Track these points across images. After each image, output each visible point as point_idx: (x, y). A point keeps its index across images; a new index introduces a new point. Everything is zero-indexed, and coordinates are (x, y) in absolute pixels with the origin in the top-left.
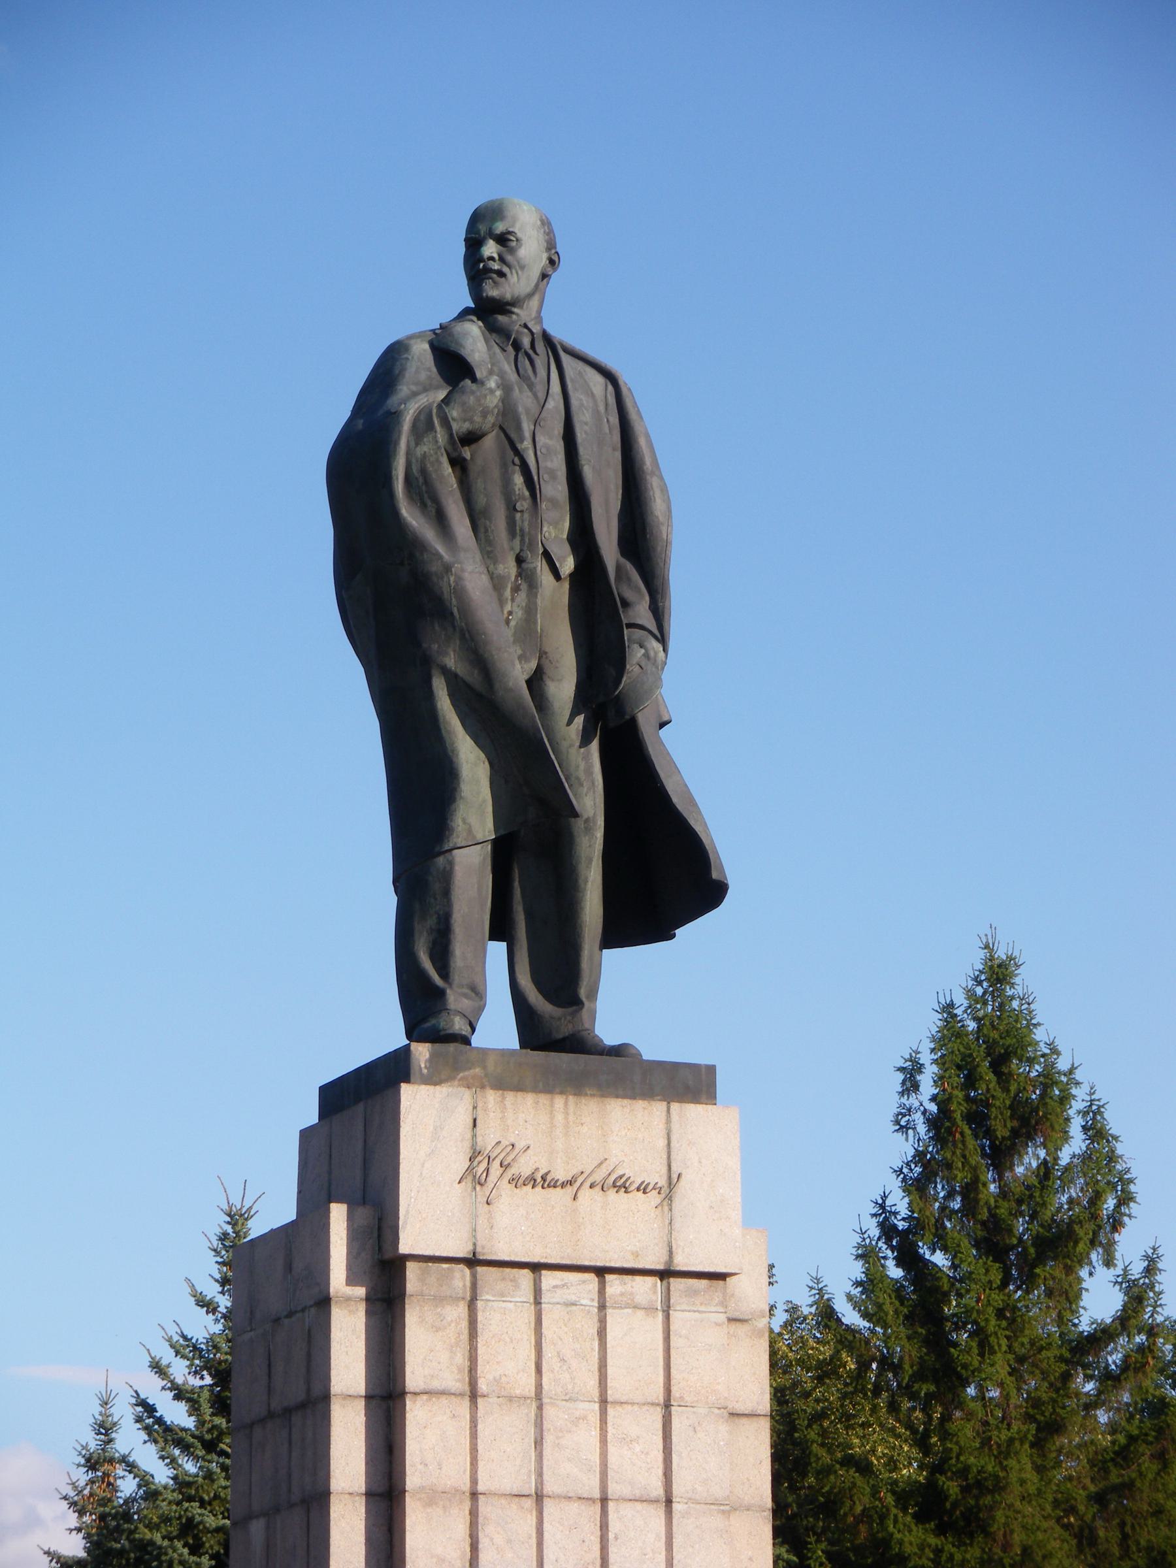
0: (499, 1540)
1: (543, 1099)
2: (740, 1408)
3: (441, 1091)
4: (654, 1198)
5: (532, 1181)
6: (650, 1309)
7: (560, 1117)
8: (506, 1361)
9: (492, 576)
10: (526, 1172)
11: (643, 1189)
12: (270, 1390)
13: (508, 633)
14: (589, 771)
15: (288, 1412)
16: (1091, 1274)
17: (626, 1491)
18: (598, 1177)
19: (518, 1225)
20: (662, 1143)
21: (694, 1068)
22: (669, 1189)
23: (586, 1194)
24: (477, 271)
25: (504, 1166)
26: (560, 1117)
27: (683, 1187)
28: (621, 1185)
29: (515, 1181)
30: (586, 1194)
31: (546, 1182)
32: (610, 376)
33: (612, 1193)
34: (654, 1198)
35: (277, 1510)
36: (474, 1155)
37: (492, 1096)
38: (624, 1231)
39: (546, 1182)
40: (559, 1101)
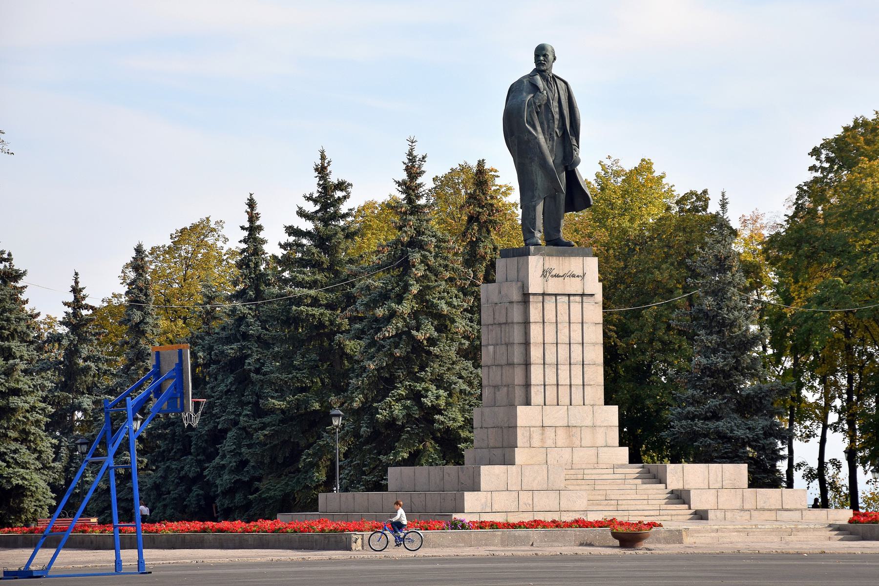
15: (500, 324)
24: (537, 61)
28: (574, 276)
29: (552, 276)
31: (558, 276)
39: (557, 276)
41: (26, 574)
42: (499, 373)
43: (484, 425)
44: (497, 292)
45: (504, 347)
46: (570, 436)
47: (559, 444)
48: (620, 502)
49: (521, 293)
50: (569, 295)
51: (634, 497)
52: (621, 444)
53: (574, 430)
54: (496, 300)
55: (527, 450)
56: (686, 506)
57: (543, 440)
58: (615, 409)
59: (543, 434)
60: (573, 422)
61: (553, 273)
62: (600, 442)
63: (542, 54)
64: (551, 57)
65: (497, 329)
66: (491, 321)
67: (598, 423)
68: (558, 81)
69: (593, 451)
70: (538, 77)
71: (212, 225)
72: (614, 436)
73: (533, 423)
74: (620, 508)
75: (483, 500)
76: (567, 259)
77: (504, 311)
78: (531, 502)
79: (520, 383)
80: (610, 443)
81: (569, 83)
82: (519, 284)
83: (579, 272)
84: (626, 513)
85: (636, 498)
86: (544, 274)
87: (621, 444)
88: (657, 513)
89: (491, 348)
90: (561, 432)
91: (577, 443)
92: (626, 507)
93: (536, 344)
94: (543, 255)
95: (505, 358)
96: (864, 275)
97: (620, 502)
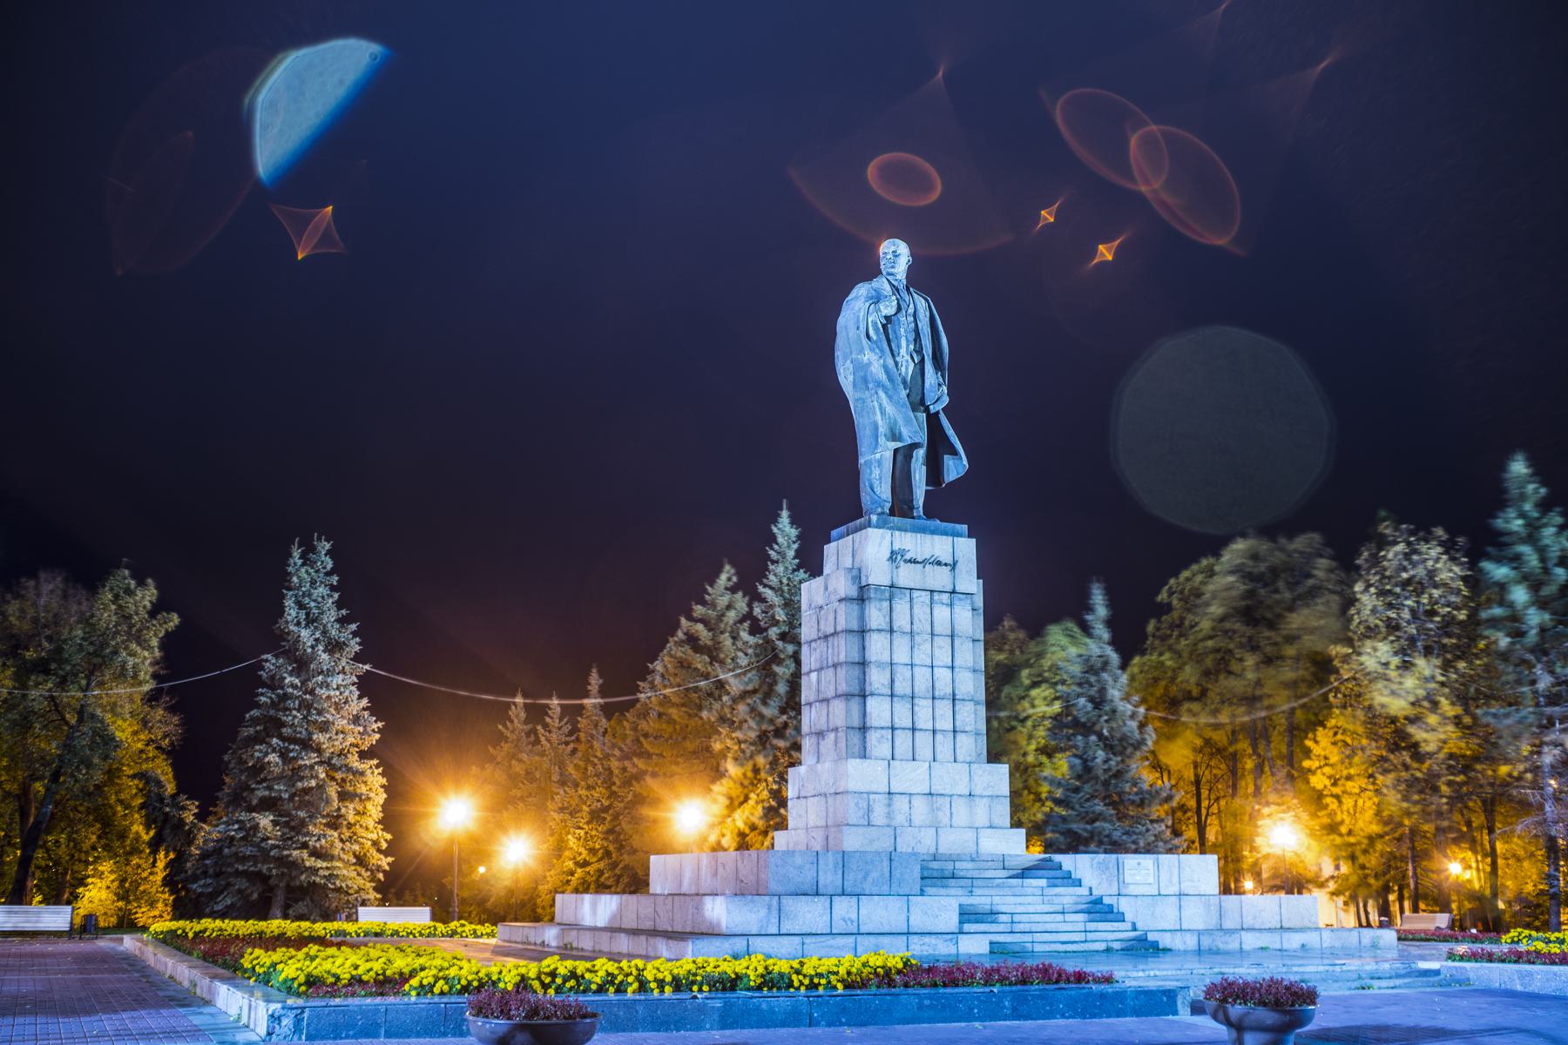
15: (826, 637)
19: (907, 576)
28: (939, 563)
31: (915, 562)
39: (915, 562)
41: (1031, 983)
42: (824, 712)
43: (803, 794)
45: (831, 670)
46: (934, 810)
47: (917, 820)
51: (1040, 908)
53: (940, 799)
54: (821, 602)
55: (861, 830)
57: (889, 816)
58: (1004, 769)
61: (908, 557)
65: (821, 645)
66: (814, 635)
71: (494, 978)
73: (874, 788)
74: (1018, 928)
77: (831, 617)
78: (854, 916)
80: (996, 821)
83: (947, 559)
84: (1027, 938)
85: (1044, 916)
86: (894, 556)
88: (1081, 937)
89: (814, 676)
90: (920, 805)
91: (946, 820)
92: (1027, 927)
93: (880, 665)
94: (891, 528)
95: (832, 687)
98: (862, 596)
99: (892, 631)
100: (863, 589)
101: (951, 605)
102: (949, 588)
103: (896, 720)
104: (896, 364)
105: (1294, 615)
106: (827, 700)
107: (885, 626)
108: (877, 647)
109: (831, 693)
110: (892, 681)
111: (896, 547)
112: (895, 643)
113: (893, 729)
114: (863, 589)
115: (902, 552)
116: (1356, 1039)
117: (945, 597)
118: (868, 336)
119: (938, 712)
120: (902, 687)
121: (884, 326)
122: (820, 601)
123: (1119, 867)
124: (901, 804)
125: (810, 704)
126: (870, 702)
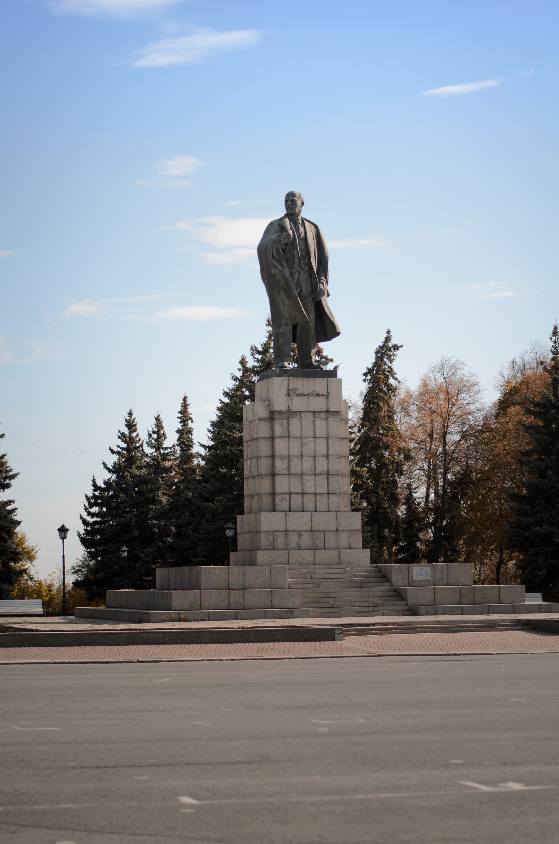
0: (143, 650)
1: (302, 378)
2: (343, 437)
3: (282, 378)
4: (325, 397)
5: (300, 395)
6: (324, 419)
7: (305, 382)
8: (295, 429)
9: (290, 272)
10: (299, 393)
11: (323, 395)
12: (250, 435)
13: (293, 283)
14: (312, 310)
15: (254, 440)
16: (192, 422)
17: (319, 454)
18: (313, 393)
19: (297, 404)
20: (326, 386)
21: (333, 326)
22: (328, 396)
23: (311, 397)
24: (288, 207)
25: (295, 392)
26: (305, 382)
27: (331, 395)
28: (318, 395)
29: (297, 395)
30: (311, 397)
31: (303, 395)
32: (316, 226)
33: (316, 397)
34: (325, 397)
35: (252, 458)
36: (288, 390)
37: (291, 378)
38: (319, 404)
39: (303, 395)
40: (305, 379)
44: (251, 411)
48: (338, 600)
49: (268, 411)
50: (314, 412)
52: (364, 547)
56: (404, 603)
59: (286, 538)
60: (316, 527)
61: (298, 392)
62: (344, 542)
63: (292, 201)
64: (299, 203)
67: (341, 528)
68: (305, 222)
69: (335, 553)
70: (287, 220)
72: (358, 540)
73: (277, 528)
75: (192, 599)
76: (311, 380)
78: (241, 600)
79: (268, 492)
80: (353, 545)
81: (320, 227)
82: (267, 403)
87: (364, 547)
89: (249, 461)
93: (282, 457)
96: (293, 277)
97: (338, 600)
98: (272, 416)
99: (289, 437)
100: (272, 412)
101: (327, 419)
102: (325, 409)
103: (292, 488)
104: (292, 274)
105: (27, 543)
106: (254, 477)
107: (286, 435)
108: (281, 446)
109: (256, 474)
110: (289, 466)
111: (291, 387)
112: (291, 444)
113: (290, 494)
114: (272, 412)
115: (295, 390)
116: (115, 620)
117: (322, 415)
118: (273, 256)
119: (318, 483)
120: (295, 469)
121: (284, 250)
122: (251, 419)
123: (409, 570)
124: (294, 537)
125: (247, 478)
126: (278, 479)
